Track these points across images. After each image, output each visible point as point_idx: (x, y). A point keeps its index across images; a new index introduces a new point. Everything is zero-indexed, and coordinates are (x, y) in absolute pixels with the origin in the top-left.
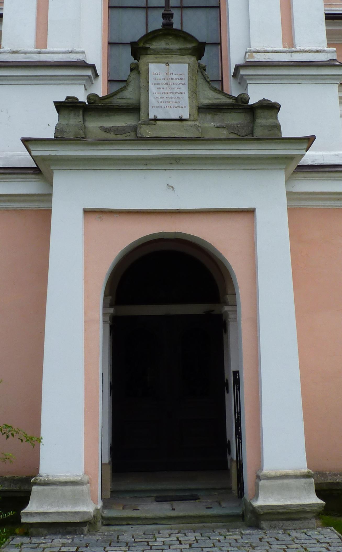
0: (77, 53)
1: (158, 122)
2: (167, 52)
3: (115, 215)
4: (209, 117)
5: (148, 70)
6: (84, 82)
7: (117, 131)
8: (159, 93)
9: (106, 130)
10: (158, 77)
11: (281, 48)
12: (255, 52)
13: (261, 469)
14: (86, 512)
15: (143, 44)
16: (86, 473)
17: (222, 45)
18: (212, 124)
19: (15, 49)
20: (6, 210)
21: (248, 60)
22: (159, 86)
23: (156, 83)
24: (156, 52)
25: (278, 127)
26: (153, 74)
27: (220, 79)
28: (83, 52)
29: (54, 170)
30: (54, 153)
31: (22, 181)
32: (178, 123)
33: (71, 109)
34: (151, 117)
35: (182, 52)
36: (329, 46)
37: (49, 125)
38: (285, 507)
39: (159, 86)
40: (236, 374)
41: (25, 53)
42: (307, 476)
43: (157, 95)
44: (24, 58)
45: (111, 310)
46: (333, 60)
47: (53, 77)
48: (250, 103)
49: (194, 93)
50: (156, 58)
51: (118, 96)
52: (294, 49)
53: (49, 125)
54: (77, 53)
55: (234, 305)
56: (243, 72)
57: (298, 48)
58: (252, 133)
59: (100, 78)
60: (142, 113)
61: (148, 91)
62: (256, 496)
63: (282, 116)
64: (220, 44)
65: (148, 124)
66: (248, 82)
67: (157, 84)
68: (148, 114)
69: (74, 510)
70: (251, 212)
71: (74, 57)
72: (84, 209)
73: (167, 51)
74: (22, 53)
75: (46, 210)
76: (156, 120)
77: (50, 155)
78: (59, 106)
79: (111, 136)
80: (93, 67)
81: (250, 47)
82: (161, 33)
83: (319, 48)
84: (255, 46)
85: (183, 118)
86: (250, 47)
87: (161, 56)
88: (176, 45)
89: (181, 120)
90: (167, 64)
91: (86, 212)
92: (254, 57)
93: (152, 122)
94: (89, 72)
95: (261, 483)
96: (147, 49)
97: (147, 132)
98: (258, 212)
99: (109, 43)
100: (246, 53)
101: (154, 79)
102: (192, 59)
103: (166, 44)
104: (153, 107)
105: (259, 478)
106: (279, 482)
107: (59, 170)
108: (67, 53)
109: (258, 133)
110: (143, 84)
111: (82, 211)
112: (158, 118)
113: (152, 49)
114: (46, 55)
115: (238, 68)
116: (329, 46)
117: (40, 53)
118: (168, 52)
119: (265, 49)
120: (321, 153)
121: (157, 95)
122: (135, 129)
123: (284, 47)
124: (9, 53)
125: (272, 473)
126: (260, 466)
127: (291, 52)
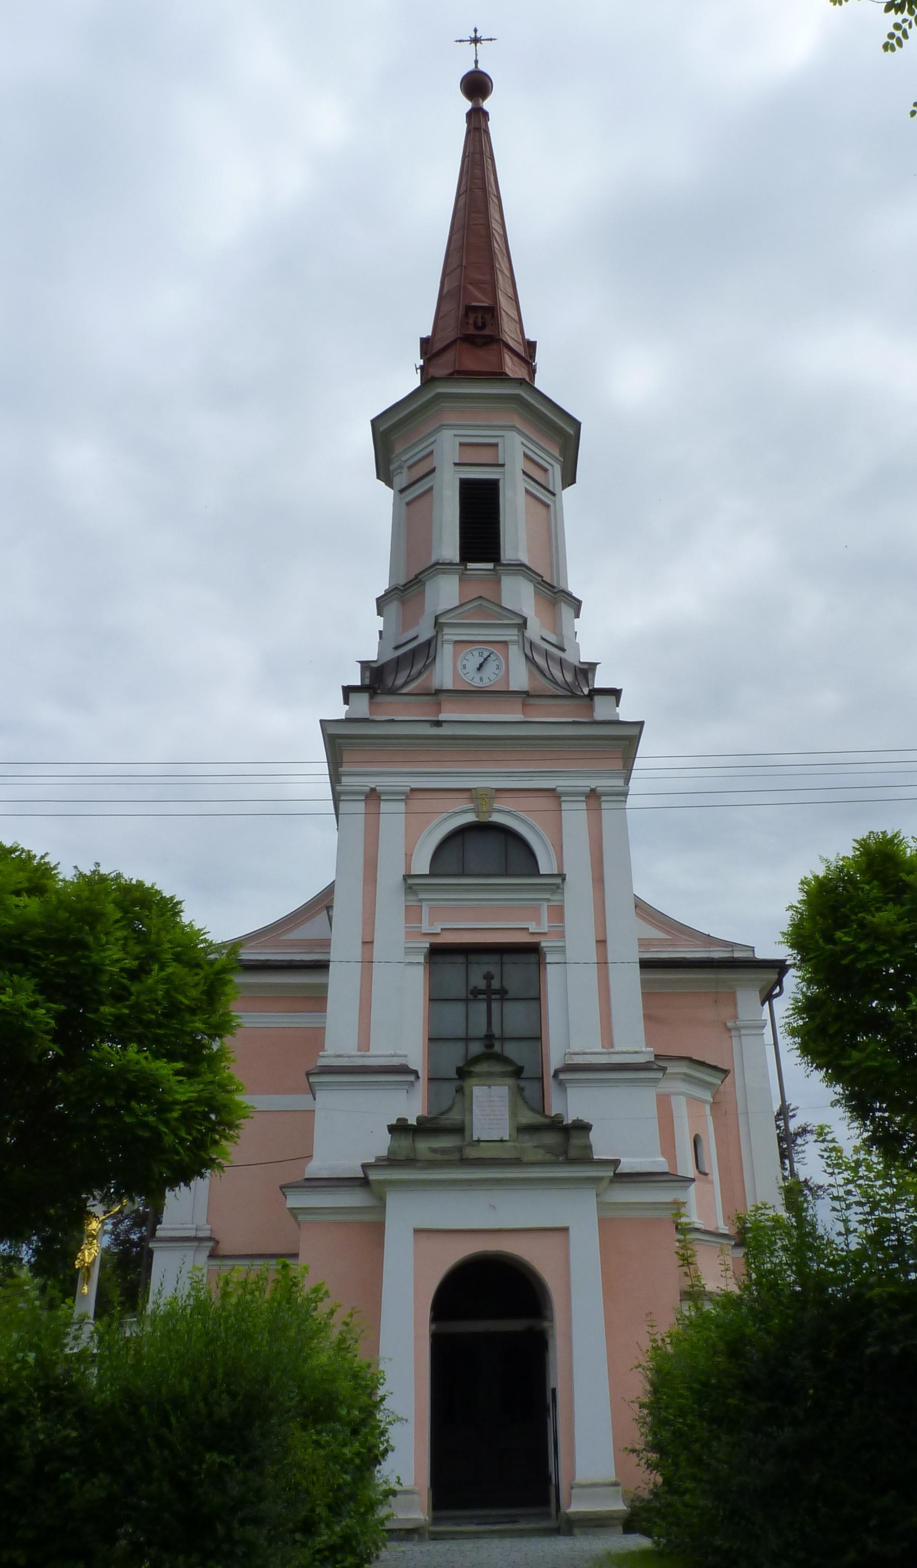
0: (400, 1056)
1: (482, 1144)
4: (527, 1137)
5: (472, 1092)
6: (407, 1087)
7: (443, 1151)
9: (434, 1151)
11: (600, 1050)
12: (574, 1054)
13: (574, 1480)
14: (418, 1519)
16: (415, 1484)
17: (543, 1040)
18: (530, 1144)
19: (339, 1053)
21: (567, 1063)
24: (479, 1075)
25: (589, 1147)
27: (541, 1076)
30: (388, 1177)
32: (500, 1144)
34: (475, 1138)
35: (503, 1075)
36: (647, 1046)
38: (595, 1513)
40: (554, 1391)
41: (349, 1057)
42: (616, 1484)
45: (546, 1324)
46: (651, 1062)
48: (565, 1123)
49: (514, 1114)
52: (611, 1050)
54: (400, 1056)
55: (552, 1321)
56: (562, 1076)
57: (617, 1049)
58: (566, 1152)
59: (421, 1079)
60: (467, 1132)
61: (472, 1112)
62: (569, 1506)
63: (593, 1136)
64: (541, 1038)
65: (473, 1146)
66: (567, 1085)
68: (472, 1136)
69: (406, 1517)
70: (565, 1230)
71: (396, 1062)
72: (414, 1229)
76: (479, 1141)
78: (392, 1129)
79: (438, 1157)
80: (415, 1073)
81: (569, 1048)
83: (637, 1050)
84: (575, 1048)
85: (504, 1139)
86: (569, 1048)
88: (497, 1068)
89: (502, 1141)
90: (489, 1086)
91: (417, 1231)
92: (573, 1060)
93: (476, 1143)
94: (412, 1078)
95: (574, 1491)
96: (472, 1072)
97: (471, 1153)
98: (572, 1231)
99: (429, 1039)
100: (566, 1054)
102: (511, 1081)
105: (572, 1488)
106: (589, 1490)
109: (573, 1153)
111: (412, 1230)
112: (482, 1139)
115: (557, 1073)
116: (647, 1046)
117: (363, 1056)
118: (490, 1074)
119: (584, 1051)
120: (638, 1160)
122: (460, 1149)
123: (603, 1047)
125: (584, 1482)
126: (573, 1477)
127: (609, 1053)
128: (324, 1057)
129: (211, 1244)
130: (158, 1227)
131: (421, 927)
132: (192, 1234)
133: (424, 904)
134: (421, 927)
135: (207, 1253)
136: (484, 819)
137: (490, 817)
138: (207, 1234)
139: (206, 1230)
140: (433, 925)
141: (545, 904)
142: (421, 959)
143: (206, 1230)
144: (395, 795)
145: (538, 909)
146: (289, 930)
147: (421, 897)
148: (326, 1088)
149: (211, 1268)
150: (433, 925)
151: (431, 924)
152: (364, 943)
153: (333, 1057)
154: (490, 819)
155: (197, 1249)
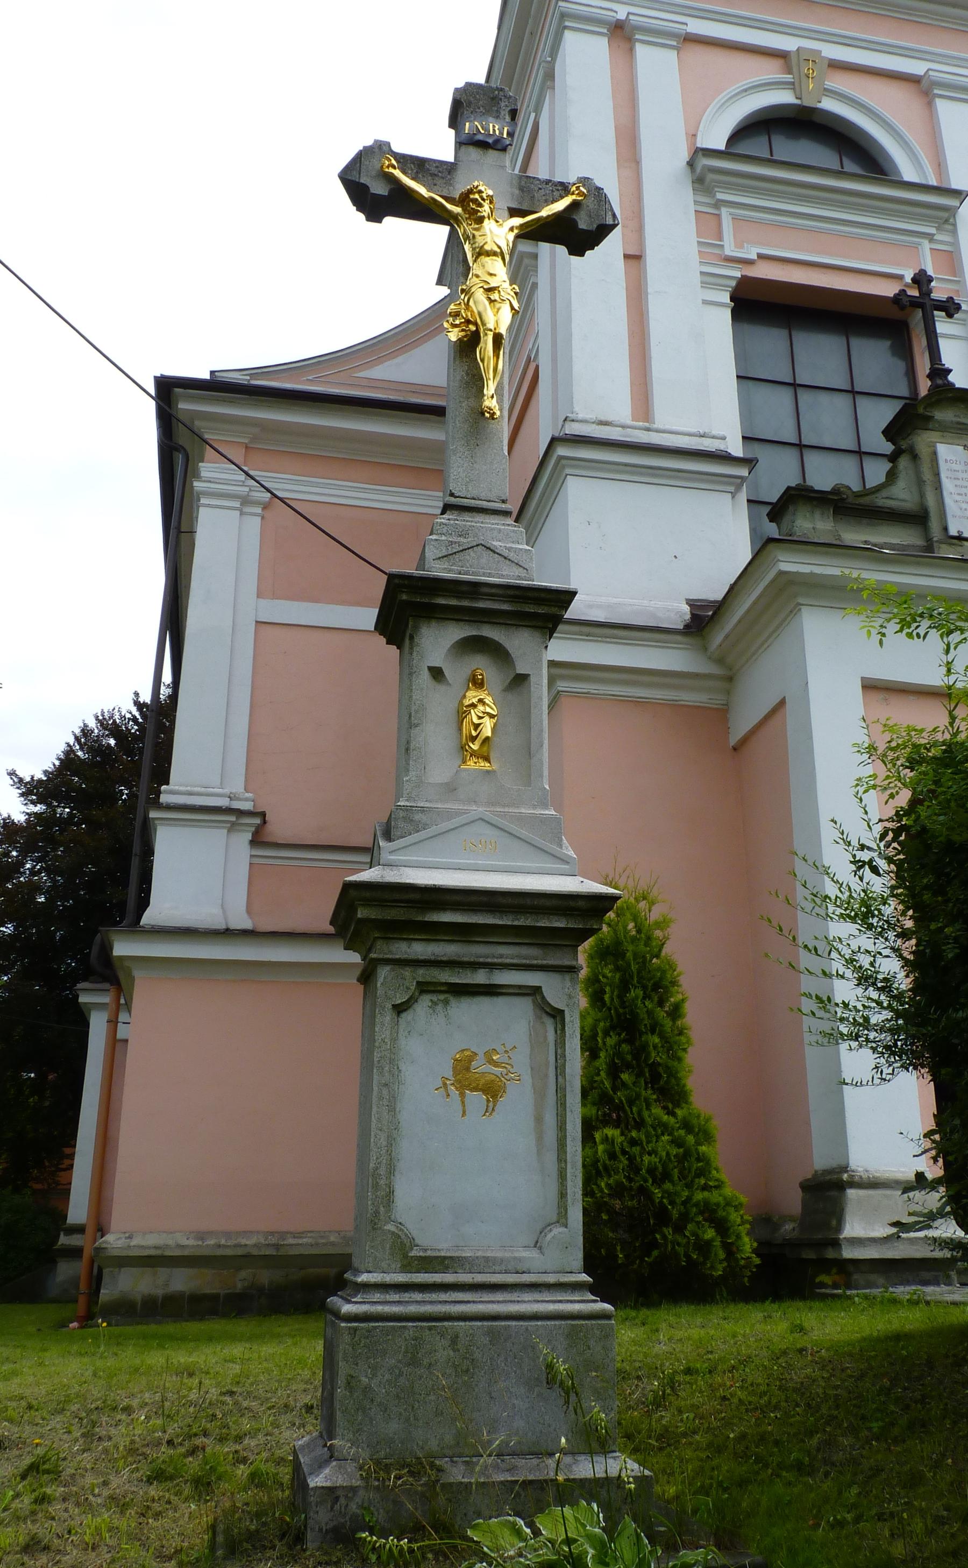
0: (713, 437)
2: (960, 429)
3: (912, 698)
5: (935, 453)
8: (959, 494)
10: (954, 466)
15: (925, 408)
19: (603, 418)
20: (622, 700)
22: (958, 483)
23: (953, 477)
26: (946, 461)
28: (724, 438)
29: (803, 605)
31: (656, 646)
33: (815, 503)
37: (675, 557)
39: (958, 483)
43: (958, 498)
44: (621, 436)
47: (680, 474)
50: (943, 436)
51: (884, 493)
53: (675, 557)
54: (713, 437)
67: (955, 479)
73: (959, 426)
74: (617, 426)
75: (699, 707)
77: (812, 574)
82: (951, 395)
87: (951, 435)
91: (871, 687)
101: (948, 469)
103: (955, 416)
104: (954, 516)
107: (811, 605)
108: (696, 436)
110: (927, 475)
113: (938, 422)
114: (661, 434)
121: (958, 498)
124: (593, 423)
128: (577, 421)
129: (258, 821)
130: (163, 788)
131: (722, 246)
132: (223, 802)
133: (724, 212)
134: (722, 246)
135: (249, 836)
136: (808, 102)
137: (820, 102)
138: (247, 806)
139: (247, 800)
140: (742, 247)
141: (926, 245)
142: (725, 298)
143: (247, 800)
144: (659, 36)
145: (916, 247)
146: (380, 360)
147: (720, 196)
148: (584, 473)
149: (256, 860)
150: (742, 247)
151: (739, 245)
152: (627, 257)
153: (593, 423)
154: (820, 105)
155: (233, 828)
